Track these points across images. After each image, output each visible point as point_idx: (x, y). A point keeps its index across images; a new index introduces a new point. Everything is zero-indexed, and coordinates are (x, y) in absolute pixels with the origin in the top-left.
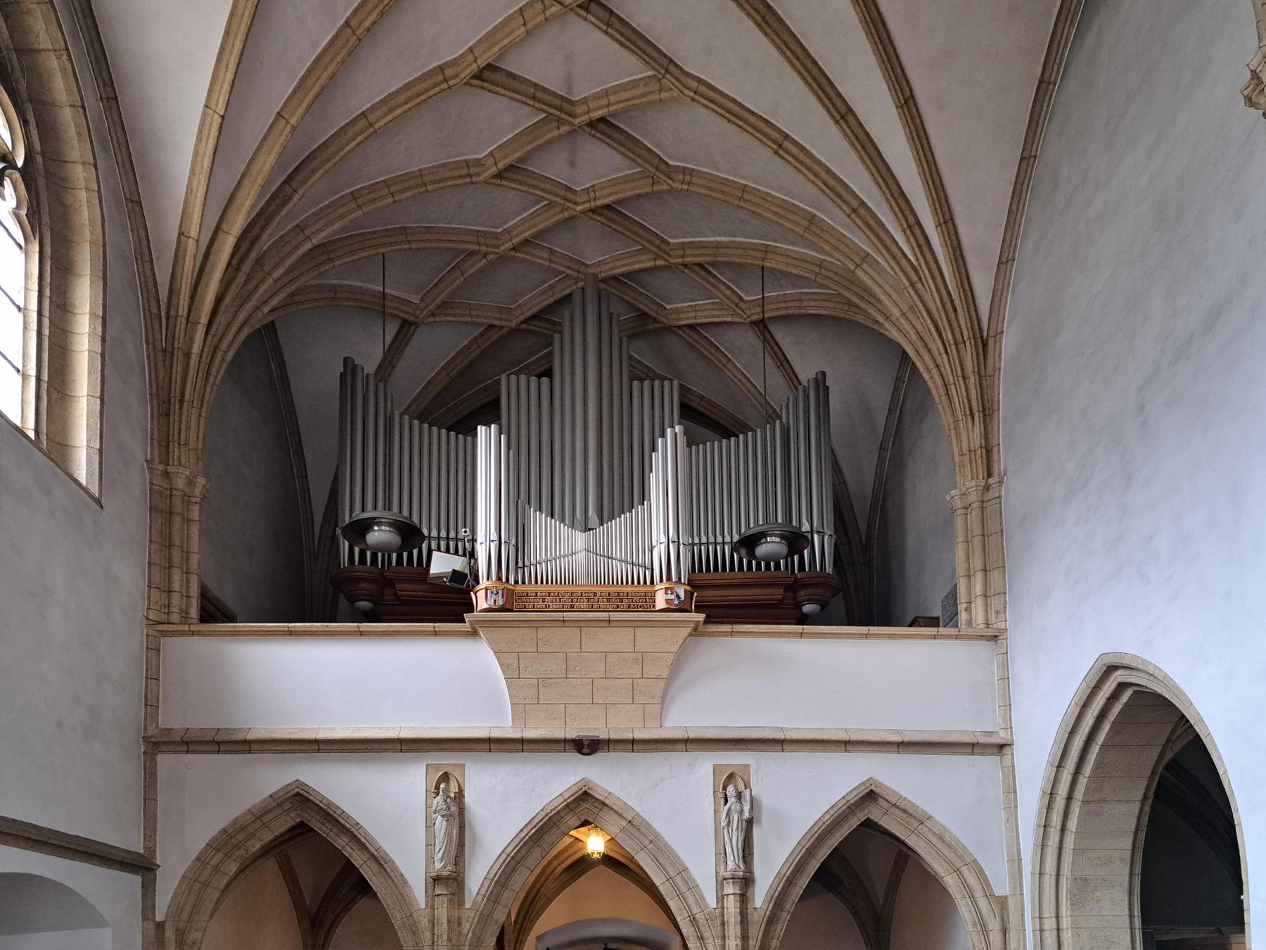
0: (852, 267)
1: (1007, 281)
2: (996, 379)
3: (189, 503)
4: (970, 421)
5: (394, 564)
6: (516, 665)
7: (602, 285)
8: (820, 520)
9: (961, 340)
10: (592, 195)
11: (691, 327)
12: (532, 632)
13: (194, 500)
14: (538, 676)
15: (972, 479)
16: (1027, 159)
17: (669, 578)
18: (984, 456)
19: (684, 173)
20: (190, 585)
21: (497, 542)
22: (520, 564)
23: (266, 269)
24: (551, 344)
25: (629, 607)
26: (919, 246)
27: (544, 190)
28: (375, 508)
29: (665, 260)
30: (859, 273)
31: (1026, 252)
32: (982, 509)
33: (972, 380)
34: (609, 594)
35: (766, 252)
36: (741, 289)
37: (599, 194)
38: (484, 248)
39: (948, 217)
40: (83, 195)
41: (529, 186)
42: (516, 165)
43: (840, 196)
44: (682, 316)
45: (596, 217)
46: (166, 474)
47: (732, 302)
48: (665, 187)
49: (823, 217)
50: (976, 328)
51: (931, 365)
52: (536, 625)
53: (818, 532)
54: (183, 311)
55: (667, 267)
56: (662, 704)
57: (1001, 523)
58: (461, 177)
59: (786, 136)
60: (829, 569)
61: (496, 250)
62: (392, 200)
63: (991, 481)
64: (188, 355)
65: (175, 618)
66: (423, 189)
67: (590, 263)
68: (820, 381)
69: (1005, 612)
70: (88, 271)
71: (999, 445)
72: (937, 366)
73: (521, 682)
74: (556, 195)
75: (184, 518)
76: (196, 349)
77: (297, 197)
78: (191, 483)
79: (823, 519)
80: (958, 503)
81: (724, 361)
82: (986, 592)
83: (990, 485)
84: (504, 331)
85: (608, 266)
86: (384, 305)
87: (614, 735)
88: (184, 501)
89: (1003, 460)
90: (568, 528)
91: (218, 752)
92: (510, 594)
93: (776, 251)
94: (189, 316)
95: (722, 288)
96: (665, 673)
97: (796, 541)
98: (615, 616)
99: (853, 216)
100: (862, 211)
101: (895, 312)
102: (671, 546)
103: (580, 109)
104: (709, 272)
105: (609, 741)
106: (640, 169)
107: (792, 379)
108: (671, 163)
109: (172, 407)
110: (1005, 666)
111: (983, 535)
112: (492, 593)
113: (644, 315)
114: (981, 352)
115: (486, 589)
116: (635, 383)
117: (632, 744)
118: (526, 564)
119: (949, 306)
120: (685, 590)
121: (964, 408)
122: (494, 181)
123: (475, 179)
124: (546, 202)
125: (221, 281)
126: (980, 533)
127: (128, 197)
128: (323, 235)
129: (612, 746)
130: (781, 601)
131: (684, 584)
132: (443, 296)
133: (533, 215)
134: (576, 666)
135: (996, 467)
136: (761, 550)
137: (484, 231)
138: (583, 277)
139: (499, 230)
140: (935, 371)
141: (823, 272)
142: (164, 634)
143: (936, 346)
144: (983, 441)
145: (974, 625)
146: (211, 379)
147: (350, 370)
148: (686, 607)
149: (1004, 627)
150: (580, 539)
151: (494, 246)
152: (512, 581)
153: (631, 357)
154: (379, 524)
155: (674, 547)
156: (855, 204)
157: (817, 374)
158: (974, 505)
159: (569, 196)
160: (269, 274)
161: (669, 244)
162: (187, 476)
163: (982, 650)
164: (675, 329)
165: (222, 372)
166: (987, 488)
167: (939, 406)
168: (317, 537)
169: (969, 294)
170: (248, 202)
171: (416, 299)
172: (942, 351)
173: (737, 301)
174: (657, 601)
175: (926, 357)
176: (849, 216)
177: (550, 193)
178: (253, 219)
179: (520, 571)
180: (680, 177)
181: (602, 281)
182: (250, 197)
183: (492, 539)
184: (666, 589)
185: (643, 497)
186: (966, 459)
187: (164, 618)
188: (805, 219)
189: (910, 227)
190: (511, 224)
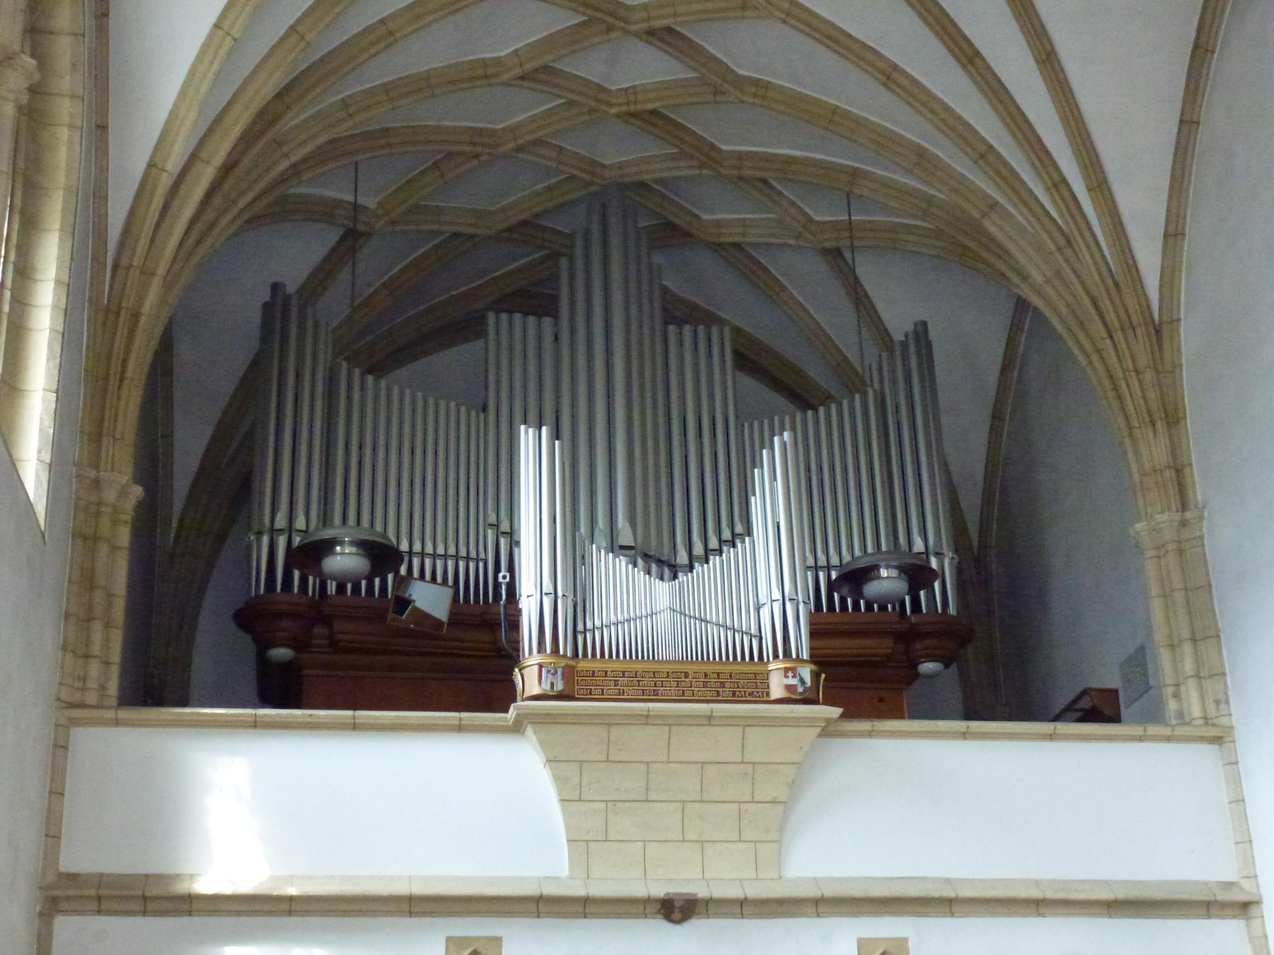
0: (976, 215)
4: (1150, 430)
6: (576, 780)
10: (632, 97)
12: (602, 731)
16: (1188, 124)
17: (787, 653)
20: (111, 645)
21: (553, 595)
22: (580, 627)
31: (1198, 228)
32: (1181, 552)
34: (706, 675)
37: (640, 97)
40: (64, 134)
44: (724, 231)
46: (97, 483)
52: (608, 721)
59: (895, 67)
60: (952, 610)
63: (1188, 515)
64: (136, 316)
65: (92, 698)
68: (921, 334)
69: (1227, 702)
70: (57, 225)
87: (720, 892)
89: (1200, 490)
90: (607, 553)
91: (144, 913)
92: (570, 674)
93: (866, 175)
97: (918, 575)
99: (981, 162)
102: (788, 605)
103: (636, 16)
105: (708, 902)
107: (883, 334)
110: (1235, 781)
112: (548, 672)
115: (541, 666)
116: (672, 328)
117: (743, 907)
120: (811, 671)
126: (1181, 585)
129: (746, 910)
130: (888, 657)
135: (1191, 496)
136: (872, 589)
140: (1095, 357)
142: (74, 722)
143: (1097, 328)
154: (341, 543)
156: (982, 148)
157: (916, 325)
159: (602, 96)
161: (720, 150)
166: (1184, 524)
180: (753, 89)
184: (786, 670)
185: (749, 532)
187: (77, 697)
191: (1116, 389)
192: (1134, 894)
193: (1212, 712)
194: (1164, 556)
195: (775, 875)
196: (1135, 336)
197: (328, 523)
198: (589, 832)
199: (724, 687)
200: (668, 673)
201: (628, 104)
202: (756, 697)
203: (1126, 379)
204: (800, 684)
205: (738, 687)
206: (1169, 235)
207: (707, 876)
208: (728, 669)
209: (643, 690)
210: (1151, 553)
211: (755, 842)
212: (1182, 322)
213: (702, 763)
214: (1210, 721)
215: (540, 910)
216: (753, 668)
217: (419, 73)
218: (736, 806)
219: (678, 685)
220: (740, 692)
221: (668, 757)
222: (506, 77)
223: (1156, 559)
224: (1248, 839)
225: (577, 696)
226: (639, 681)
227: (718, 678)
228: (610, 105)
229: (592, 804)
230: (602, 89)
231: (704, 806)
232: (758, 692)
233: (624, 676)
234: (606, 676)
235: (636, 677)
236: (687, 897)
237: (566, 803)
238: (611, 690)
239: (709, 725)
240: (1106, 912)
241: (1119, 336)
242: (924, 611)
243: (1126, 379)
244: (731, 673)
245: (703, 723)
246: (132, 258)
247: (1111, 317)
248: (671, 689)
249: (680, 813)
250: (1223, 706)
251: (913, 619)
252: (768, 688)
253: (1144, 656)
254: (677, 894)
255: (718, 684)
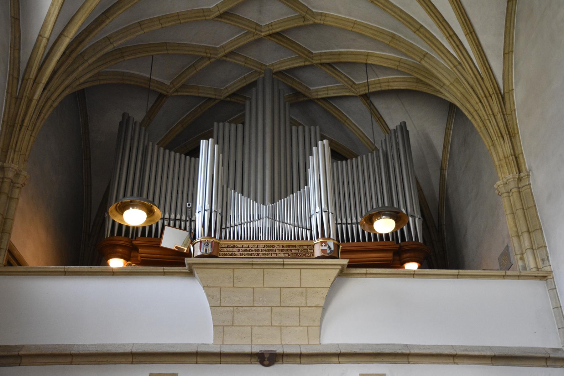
1: (510, 63)
2: (514, 116)
3: (13, 187)
4: (502, 140)
5: (139, 235)
6: (218, 296)
7: (274, 76)
8: (412, 208)
9: (489, 95)
10: (270, 27)
11: (325, 99)
12: (230, 272)
13: (17, 185)
14: (234, 305)
15: (509, 174)
18: (514, 160)
19: (321, 16)
21: (209, 211)
22: (224, 226)
23: (86, 58)
24: (244, 109)
25: (296, 255)
26: (457, 46)
27: (245, 25)
28: (132, 195)
29: (310, 61)
30: (423, 62)
32: (520, 192)
33: (499, 116)
35: (368, 55)
36: (353, 78)
37: (274, 27)
38: (209, 55)
39: (472, 30)
41: (236, 22)
42: (230, 12)
43: (409, 23)
45: (271, 38)
47: (349, 84)
48: (311, 22)
49: (400, 35)
50: (497, 88)
51: (472, 110)
53: (412, 216)
54: (32, 75)
55: (312, 66)
56: (320, 326)
57: (534, 201)
58: (200, 16)
60: (420, 240)
61: (216, 56)
62: (160, 26)
63: (522, 174)
64: (30, 100)
66: (178, 22)
67: (267, 65)
68: (403, 127)
69: (548, 259)
71: (522, 153)
72: (476, 110)
73: (221, 309)
74: (251, 28)
75: (8, 197)
76: (36, 97)
77: (108, 22)
78: (17, 174)
79: (413, 207)
80: (503, 190)
81: (345, 119)
82: (532, 246)
83: (522, 177)
84: (217, 101)
85: (278, 66)
86: (150, 85)
87: (288, 350)
88: (10, 186)
92: (216, 245)
93: (373, 55)
94: (36, 78)
95: (343, 77)
96: (322, 303)
98: (287, 261)
99: (417, 32)
100: (422, 30)
101: (447, 83)
102: (324, 214)
104: (335, 69)
106: (297, 14)
108: (314, 10)
109: (15, 129)
111: (523, 209)
112: (204, 244)
113: (297, 94)
114: (501, 100)
115: (201, 242)
116: (294, 128)
118: (227, 226)
119: (478, 77)
120: (334, 244)
121: (497, 133)
122: (216, 19)
123: (207, 18)
124: (247, 31)
125: (59, 61)
127: (13, 15)
128: (120, 42)
131: (333, 239)
132: (182, 81)
133: (237, 39)
134: (260, 298)
135: (523, 167)
137: (210, 47)
138: (263, 71)
139: (218, 47)
140: (475, 114)
141: (401, 64)
144: (512, 151)
145: (528, 269)
146: (42, 115)
147: (126, 120)
148: (336, 255)
149: (549, 270)
150: (263, 210)
151: (214, 54)
152: (218, 236)
153: (291, 119)
155: (325, 215)
157: (401, 123)
158: (514, 190)
159: (258, 28)
160: (87, 61)
161: (312, 53)
162: (16, 170)
163: (538, 287)
164: (316, 101)
165: (49, 112)
166: (520, 179)
167: (480, 134)
168: (92, 224)
169: (489, 70)
170: (81, 21)
171: (168, 83)
172: (478, 101)
173: (352, 84)
174: (315, 251)
175: (468, 106)
176: (415, 32)
177: (248, 26)
178: (82, 31)
179: (223, 231)
181: (275, 74)
182: (82, 19)
183: (206, 209)
184: (322, 242)
185: (306, 183)
186: (503, 162)
188: (390, 36)
189: (450, 36)
190: (225, 43)
191: (485, 126)
192: (503, 353)
193: (540, 264)
194: (512, 195)
195: (318, 343)
196: (493, 100)
197: (125, 196)
198: (224, 322)
199: (292, 252)
200: (264, 245)
201: (269, 30)
202: (307, 256)
203: (489, 119)
204: (328, 249)
205: (299, 252)
206: (505, 54)
207: (283, 343)
208: (297, 243)
209: (252, 253)
210: (505, 195)
211: (308, 326)
212: (514, 91)
213: (280, 287)
214: (540, 270)
215: (198, 360)
216: (306, 243)
217: (174, 13)
218: (298, 309)
219: (269, 251)
220: (300, 254)
221: (263, 285)
222: (212, 16)
223: (508, 197)
224: (559, 306)
225: (219, 256)
226: (250, 249)
227: (289, 248)
228: (261, 32)
229: (226, 308)
230: (257, 24)
231: (281, 308)
232: (308, 254)
233: (243, 247)
234: (234, 247)
235: (249, 247)
236: (270, 352)
237: (212, 307)
238: (237, 254)
239: (283, 268)
240: (491, 362)
241: (484, 100)
242: (407, 241)
243: (489, 119)
244: (295, 246)
245: (281, 268)
246: (29, 75)
247: (480, 92)
248: (266, 253)
249: (269, 313)
250: (546, 262)
251: (403, 244)
252: (314, 252)
253: (508, 251)
254: (266, 351)
255: (289, 250)
